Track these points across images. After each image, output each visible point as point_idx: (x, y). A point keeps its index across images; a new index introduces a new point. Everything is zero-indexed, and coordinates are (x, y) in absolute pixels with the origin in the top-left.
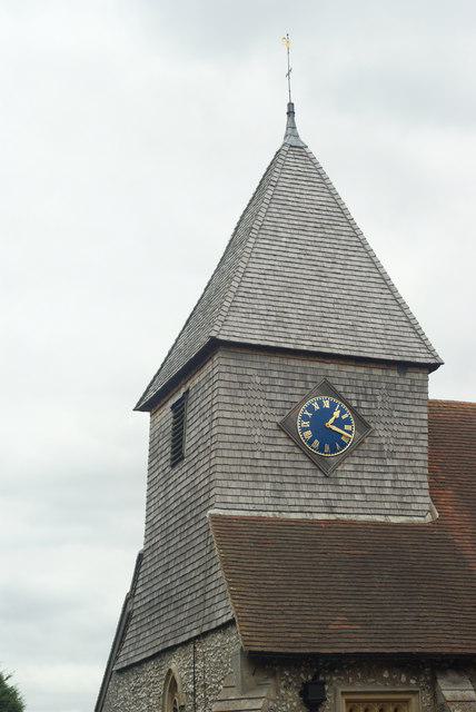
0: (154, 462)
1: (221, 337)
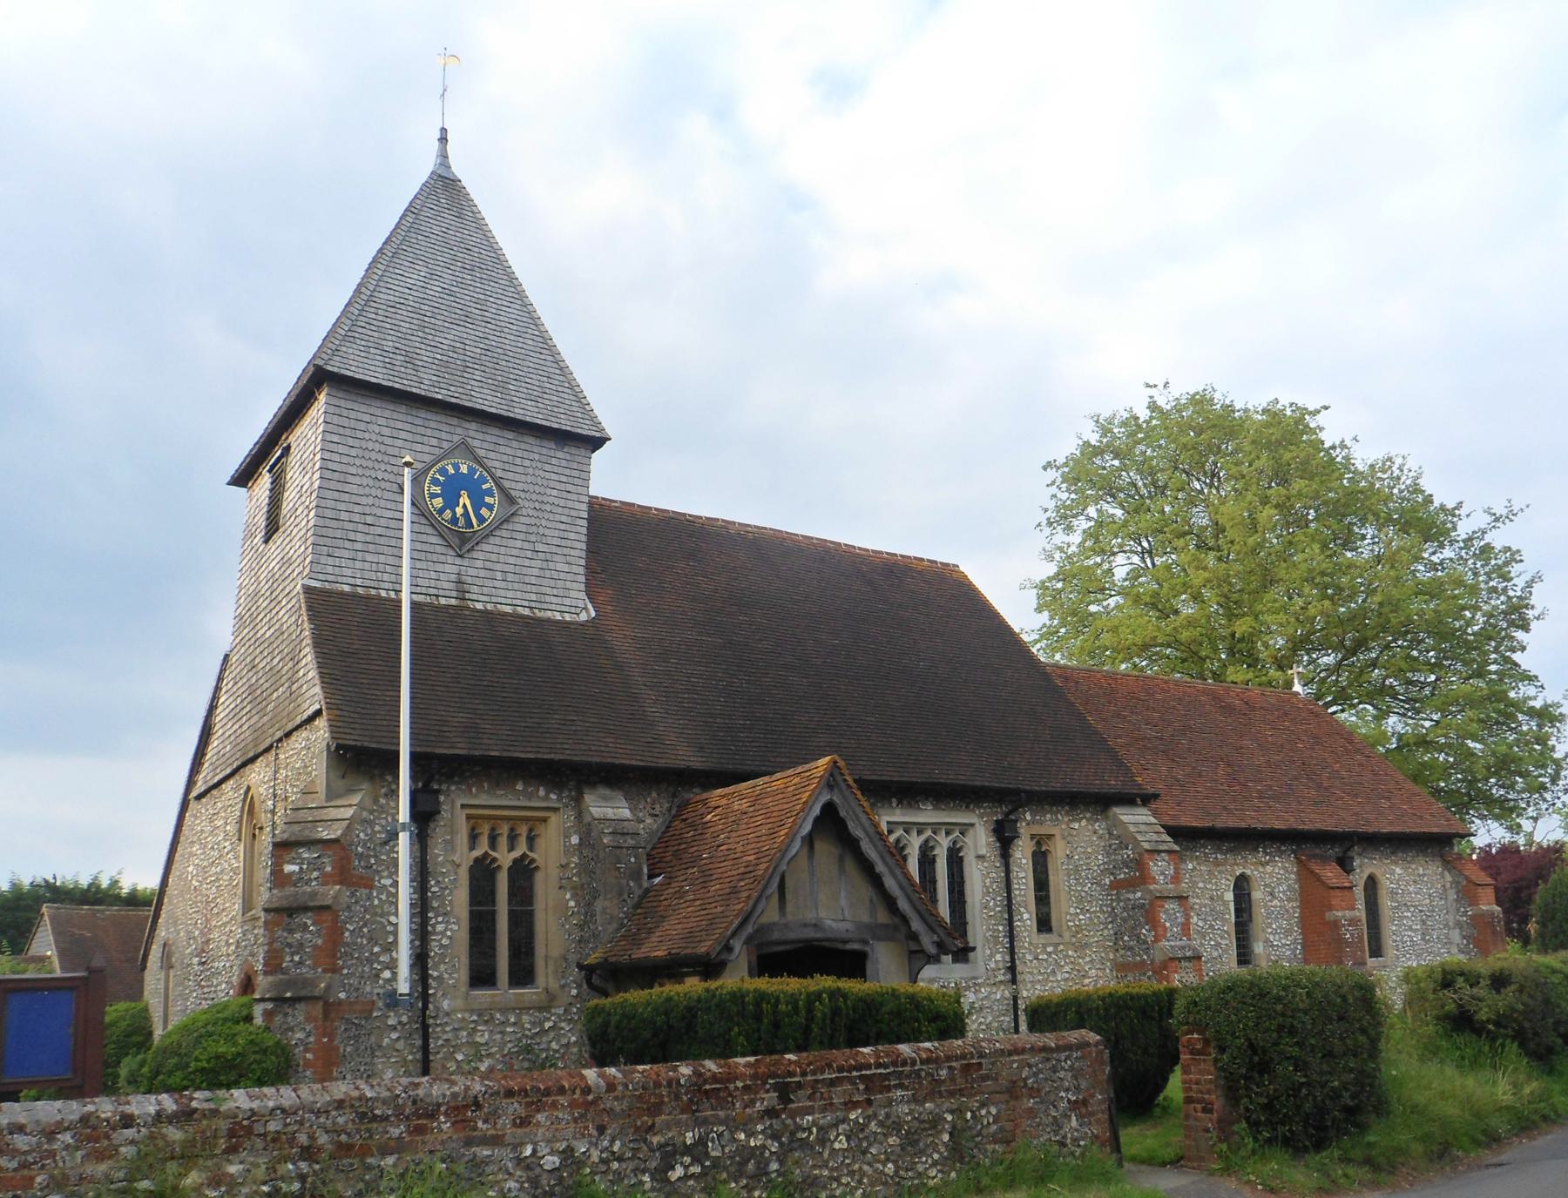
1: (329, 368)
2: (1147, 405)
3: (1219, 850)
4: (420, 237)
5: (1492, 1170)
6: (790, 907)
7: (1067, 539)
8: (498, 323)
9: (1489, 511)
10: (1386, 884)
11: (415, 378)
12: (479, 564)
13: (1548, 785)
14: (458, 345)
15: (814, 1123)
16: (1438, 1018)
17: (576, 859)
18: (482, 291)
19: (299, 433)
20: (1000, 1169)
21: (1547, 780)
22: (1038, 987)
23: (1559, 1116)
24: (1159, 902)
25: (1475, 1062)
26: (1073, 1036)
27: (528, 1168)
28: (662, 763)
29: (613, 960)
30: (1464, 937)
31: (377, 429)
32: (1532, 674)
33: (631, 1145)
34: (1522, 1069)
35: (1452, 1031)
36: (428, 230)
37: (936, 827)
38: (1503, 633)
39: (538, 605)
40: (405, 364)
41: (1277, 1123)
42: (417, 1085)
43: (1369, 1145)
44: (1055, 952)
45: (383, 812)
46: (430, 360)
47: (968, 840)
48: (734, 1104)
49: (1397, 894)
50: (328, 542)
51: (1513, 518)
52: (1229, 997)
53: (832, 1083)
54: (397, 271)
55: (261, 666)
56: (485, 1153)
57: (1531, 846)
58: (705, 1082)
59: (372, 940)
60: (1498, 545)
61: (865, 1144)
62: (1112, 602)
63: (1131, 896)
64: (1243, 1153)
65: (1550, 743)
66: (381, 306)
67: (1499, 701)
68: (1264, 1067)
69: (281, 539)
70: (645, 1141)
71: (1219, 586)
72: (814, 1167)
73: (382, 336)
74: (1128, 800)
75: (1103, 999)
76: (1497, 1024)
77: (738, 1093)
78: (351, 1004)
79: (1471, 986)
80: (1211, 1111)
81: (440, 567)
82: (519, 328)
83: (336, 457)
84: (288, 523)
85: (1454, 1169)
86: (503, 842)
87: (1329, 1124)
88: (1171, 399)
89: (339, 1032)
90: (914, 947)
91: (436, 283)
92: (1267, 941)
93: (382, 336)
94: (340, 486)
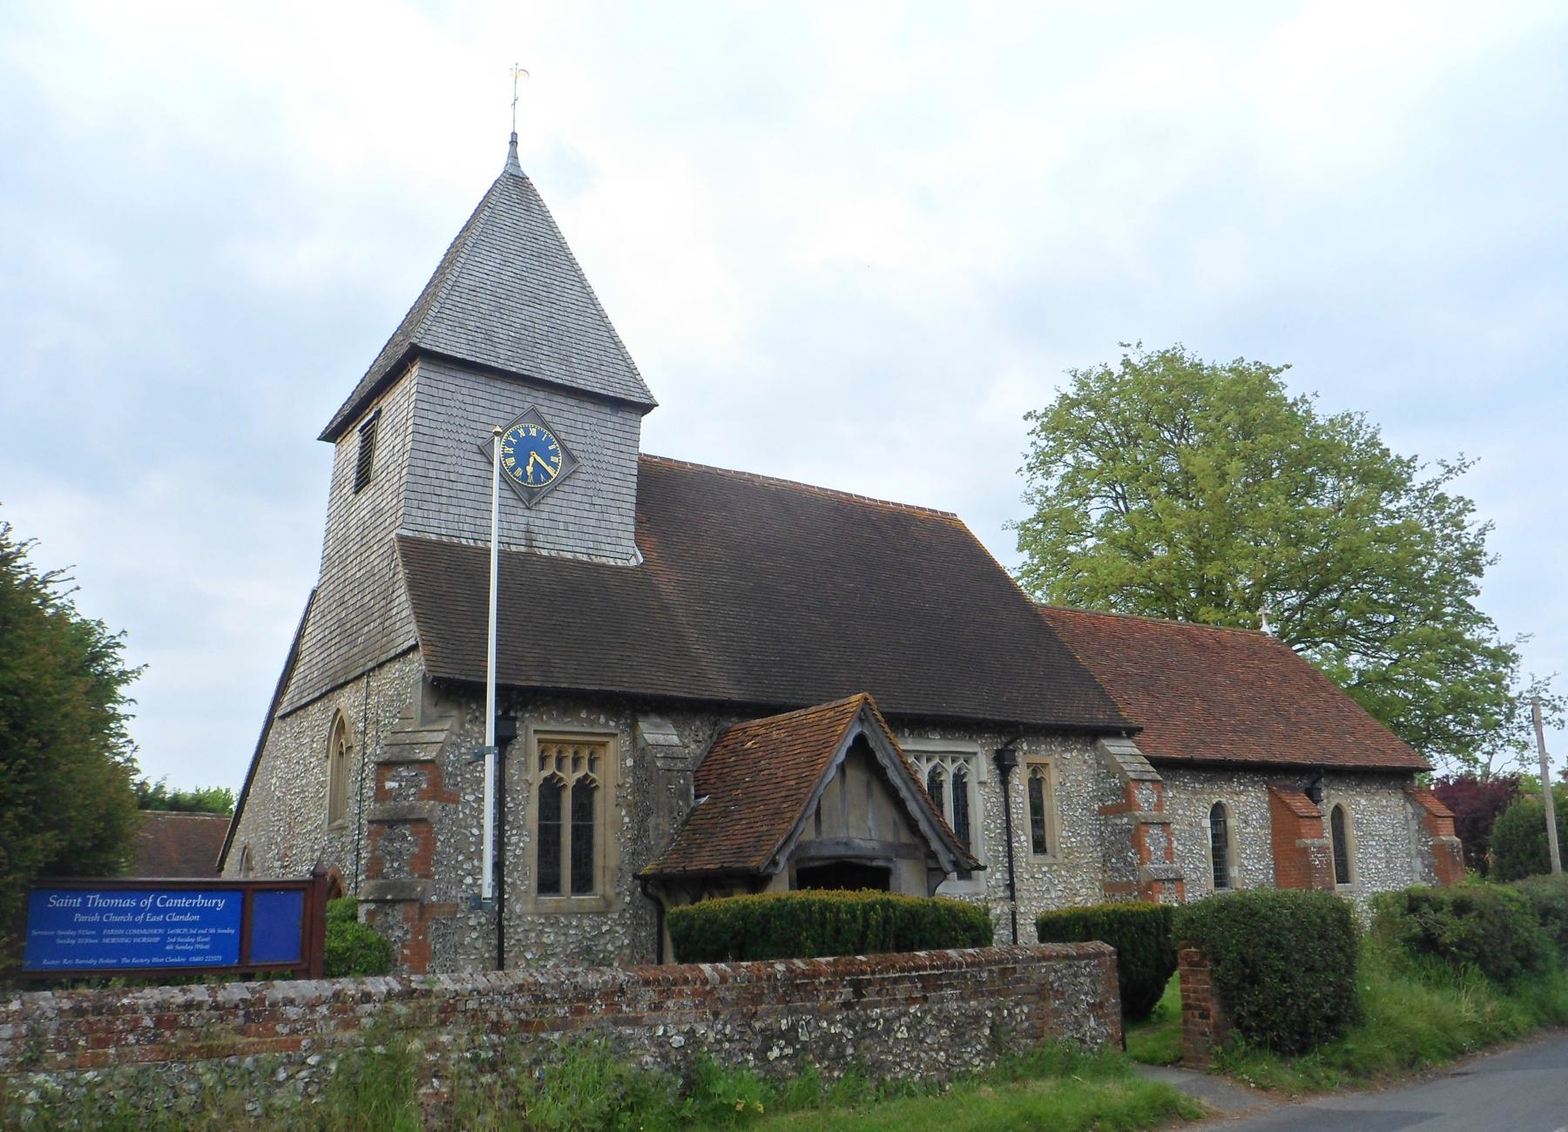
1: (422, 345)
2: (1120, 361)
4: (495, 229)
5: (1458, 1078)
6: (824, 827)
7: (1045, 483)
8: (562, 304)
9: (1442, 463)
10: (1351, 814)
11: (493, 354)
12: (544, 515)
13: (1503, 723)
14: (529, 323)
15: (882, 1015)
16: (1406, 941)
17: (630, 780)
18: (548, 276)
19: (390, 400)
20: (1031, 1060)
21: (1501, 718)
22: (1034, 903)
23: (1519, 1033)
24: (1143, 828)
25: (1441, 982)
26: (1092, 946)
27: (660, 1045)
28: (706, 695)
29: (668, 871)
30: (1426, 866)
31: (460, 398)
32: (1485, 616)
33: (739, 1029)
34: (1484, 989)
35: (1419, 952)
37: (943, 755)
38: (1458, 578)
39: (595, 552)
40: (484, 341)
41: (1266, 1029)
42: (576, 974)
43: (1347, 1052)
44: (1050, 871)
45: (468, 737)
46: (505, 337)
48: (818, 997)
49: (1362, 823)
50: (419, 496)
51: (1465, 469)
52: (1222, 916)
54: (477, 259)
55: (351, 602)
56: (628, 1032)
57: (1487, 777)
58: (796, 978)
59: (458, 850)
60: (1451, 496)
61: (922, 1035)
62: (1090, 542)
63: (1118, 822)
64: (1236, 1054)
65: (1504, 682)
66: (463, 290)
67: (1453, 643)
68: (1254, 980)
69: (372, 491)
70: (750, 1026)
71: (1191, 532)
72: (881, 1052)
73: (466, 317)
74: (1114, 733)
75: (1107, 915)
76: (1460, 947)
77: (821, 987)
78: (440, 906)
80: (1207, 1017)
81: (512, 518)
82: (580, 308)
83: (426, 422)
84: (379, 479)
86: (568, 763)
87: (1312, 1031)
88: (1143, 356)
89: (431, 931)
90: (932, 864)
91: (510, 269)
92: (1242, 865)
93: (466, 317)
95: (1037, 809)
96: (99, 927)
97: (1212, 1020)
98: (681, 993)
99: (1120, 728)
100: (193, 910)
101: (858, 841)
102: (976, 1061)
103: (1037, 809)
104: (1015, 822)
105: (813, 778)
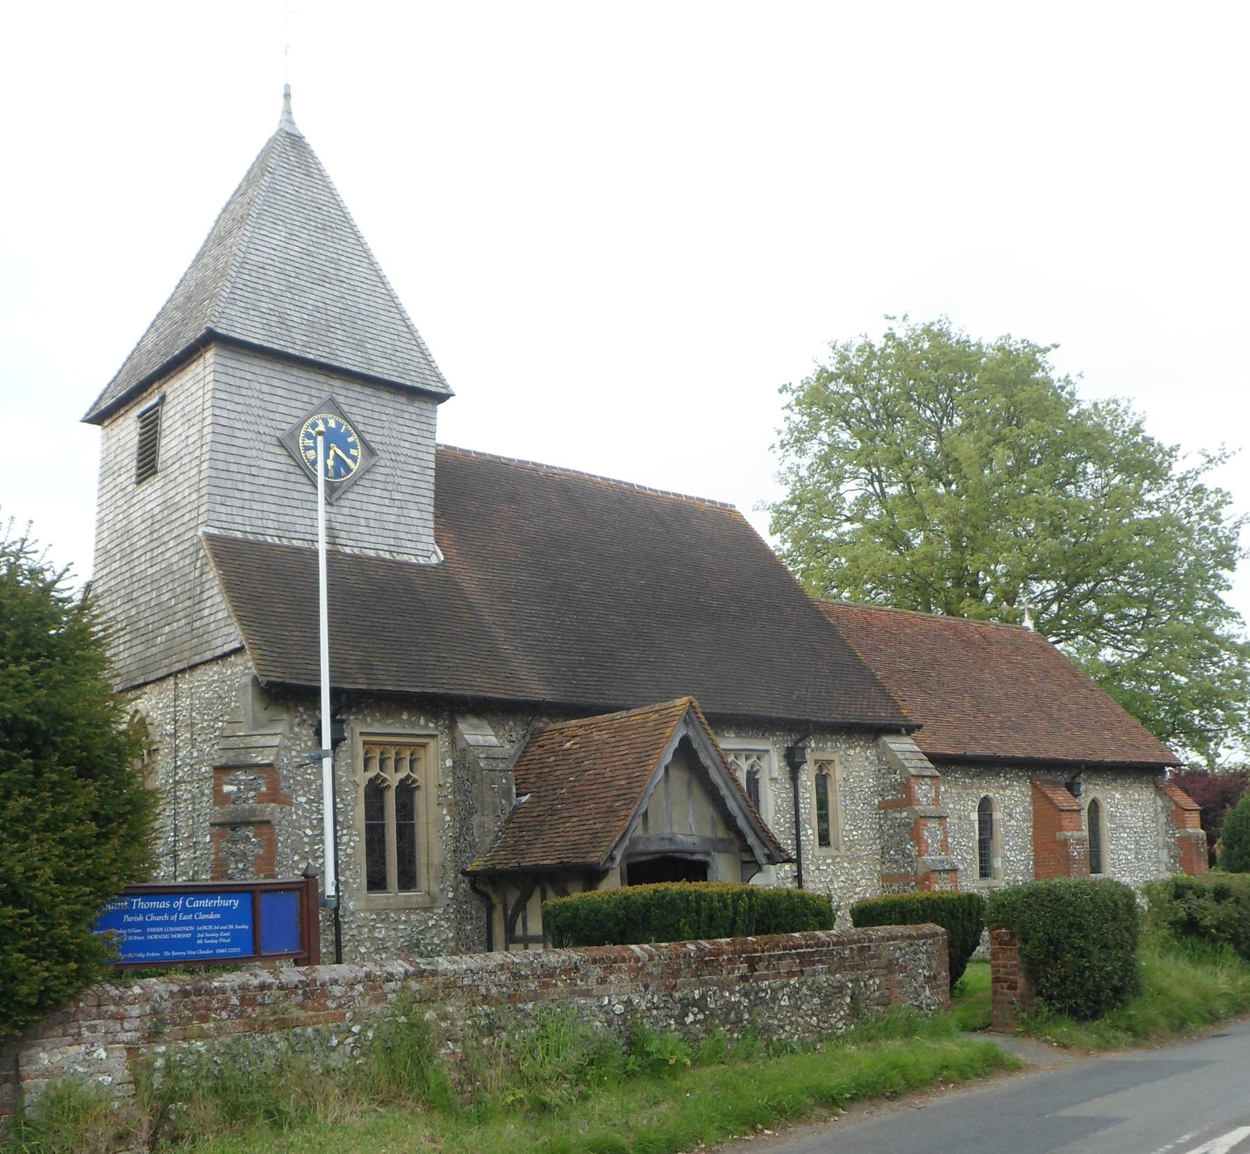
0: (106, 482)
1: (219, 330)
3: (967, 775)
4: (277, 197)
5: (1217, 1040)
6: (651, 823)
10: (1106, 808)
11: (289, 339)
12: (346, 511)
13: (1246, 718)
15: (769, 987)
17: (450, 780)
24: (923, 821)
26: (928, 927)
27: (607, 1013)
28: (521, 696)
30: (1172, 857)
31: (258, 386)
32: (1234, 611)
36: (283, 189)
43: (1130, 1017)
44: (833, 863)
46: (298, 320)
47: (764, 764)
49: (1116, 816)
50: (221, 492)
53: (780, 958)
54: (262, 232)
56: (583, 1002)
60: (1210, 487)
63: (898, 815)
64: (1039, 1019)
69: (161, 483)
70: (671, 996)
74: (894, 730)
75: (921, 902)
76: (1218, 929)
79: (1198, 897)
80: (1015, 988)
82: (369, 287)
85: (1189, 1037)
86: (391, 764)
90: (746, 857)
91: (296, 243)
92: (1005, 856)
94: (228, 440)
95: (822, 804)
96: (143, 925)
97: (1018, 992)
98: (620, 969)
99: (899, 725)
100: (216, 909)
101: (680, 836)
102: (840, 1025)
103: (822, 804)
104: (803, 817)
105: (645, 778)
